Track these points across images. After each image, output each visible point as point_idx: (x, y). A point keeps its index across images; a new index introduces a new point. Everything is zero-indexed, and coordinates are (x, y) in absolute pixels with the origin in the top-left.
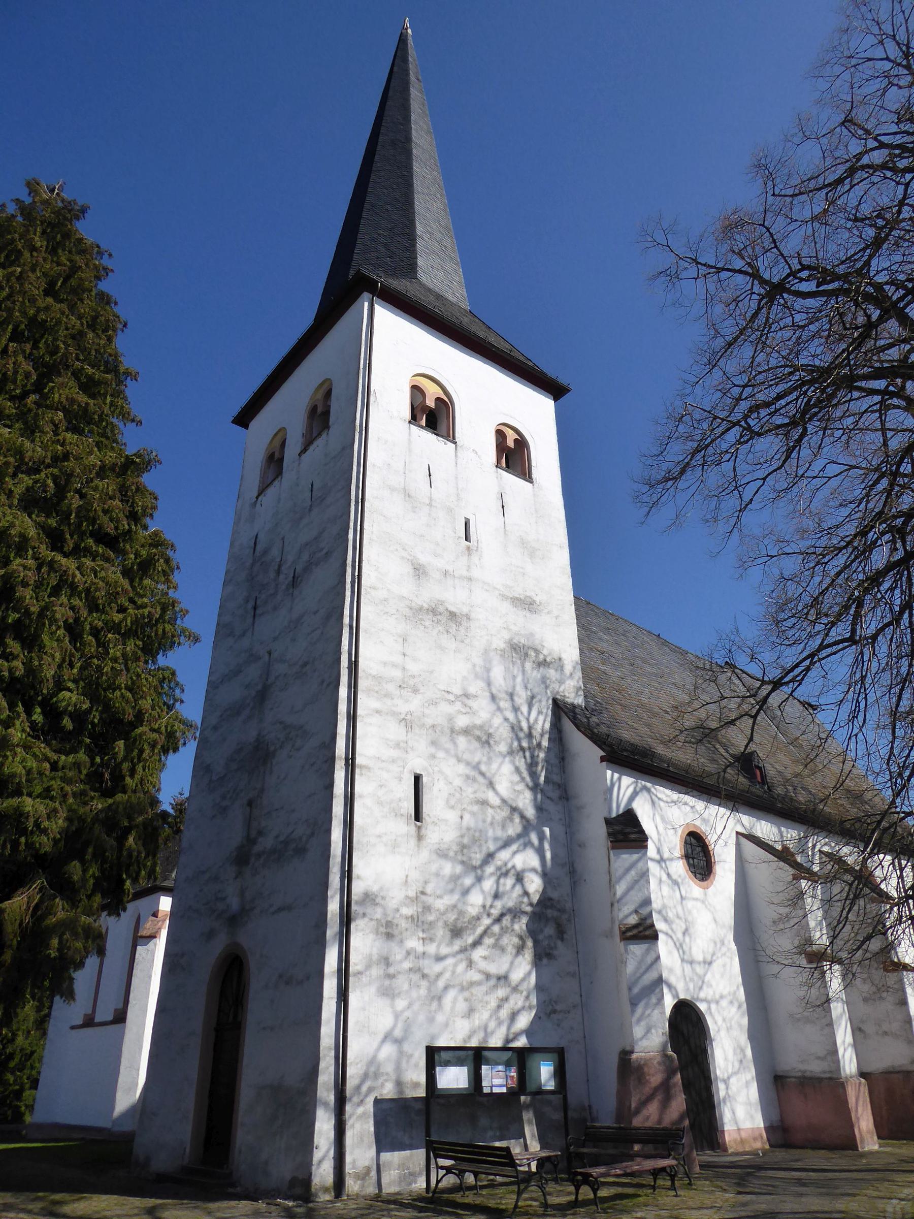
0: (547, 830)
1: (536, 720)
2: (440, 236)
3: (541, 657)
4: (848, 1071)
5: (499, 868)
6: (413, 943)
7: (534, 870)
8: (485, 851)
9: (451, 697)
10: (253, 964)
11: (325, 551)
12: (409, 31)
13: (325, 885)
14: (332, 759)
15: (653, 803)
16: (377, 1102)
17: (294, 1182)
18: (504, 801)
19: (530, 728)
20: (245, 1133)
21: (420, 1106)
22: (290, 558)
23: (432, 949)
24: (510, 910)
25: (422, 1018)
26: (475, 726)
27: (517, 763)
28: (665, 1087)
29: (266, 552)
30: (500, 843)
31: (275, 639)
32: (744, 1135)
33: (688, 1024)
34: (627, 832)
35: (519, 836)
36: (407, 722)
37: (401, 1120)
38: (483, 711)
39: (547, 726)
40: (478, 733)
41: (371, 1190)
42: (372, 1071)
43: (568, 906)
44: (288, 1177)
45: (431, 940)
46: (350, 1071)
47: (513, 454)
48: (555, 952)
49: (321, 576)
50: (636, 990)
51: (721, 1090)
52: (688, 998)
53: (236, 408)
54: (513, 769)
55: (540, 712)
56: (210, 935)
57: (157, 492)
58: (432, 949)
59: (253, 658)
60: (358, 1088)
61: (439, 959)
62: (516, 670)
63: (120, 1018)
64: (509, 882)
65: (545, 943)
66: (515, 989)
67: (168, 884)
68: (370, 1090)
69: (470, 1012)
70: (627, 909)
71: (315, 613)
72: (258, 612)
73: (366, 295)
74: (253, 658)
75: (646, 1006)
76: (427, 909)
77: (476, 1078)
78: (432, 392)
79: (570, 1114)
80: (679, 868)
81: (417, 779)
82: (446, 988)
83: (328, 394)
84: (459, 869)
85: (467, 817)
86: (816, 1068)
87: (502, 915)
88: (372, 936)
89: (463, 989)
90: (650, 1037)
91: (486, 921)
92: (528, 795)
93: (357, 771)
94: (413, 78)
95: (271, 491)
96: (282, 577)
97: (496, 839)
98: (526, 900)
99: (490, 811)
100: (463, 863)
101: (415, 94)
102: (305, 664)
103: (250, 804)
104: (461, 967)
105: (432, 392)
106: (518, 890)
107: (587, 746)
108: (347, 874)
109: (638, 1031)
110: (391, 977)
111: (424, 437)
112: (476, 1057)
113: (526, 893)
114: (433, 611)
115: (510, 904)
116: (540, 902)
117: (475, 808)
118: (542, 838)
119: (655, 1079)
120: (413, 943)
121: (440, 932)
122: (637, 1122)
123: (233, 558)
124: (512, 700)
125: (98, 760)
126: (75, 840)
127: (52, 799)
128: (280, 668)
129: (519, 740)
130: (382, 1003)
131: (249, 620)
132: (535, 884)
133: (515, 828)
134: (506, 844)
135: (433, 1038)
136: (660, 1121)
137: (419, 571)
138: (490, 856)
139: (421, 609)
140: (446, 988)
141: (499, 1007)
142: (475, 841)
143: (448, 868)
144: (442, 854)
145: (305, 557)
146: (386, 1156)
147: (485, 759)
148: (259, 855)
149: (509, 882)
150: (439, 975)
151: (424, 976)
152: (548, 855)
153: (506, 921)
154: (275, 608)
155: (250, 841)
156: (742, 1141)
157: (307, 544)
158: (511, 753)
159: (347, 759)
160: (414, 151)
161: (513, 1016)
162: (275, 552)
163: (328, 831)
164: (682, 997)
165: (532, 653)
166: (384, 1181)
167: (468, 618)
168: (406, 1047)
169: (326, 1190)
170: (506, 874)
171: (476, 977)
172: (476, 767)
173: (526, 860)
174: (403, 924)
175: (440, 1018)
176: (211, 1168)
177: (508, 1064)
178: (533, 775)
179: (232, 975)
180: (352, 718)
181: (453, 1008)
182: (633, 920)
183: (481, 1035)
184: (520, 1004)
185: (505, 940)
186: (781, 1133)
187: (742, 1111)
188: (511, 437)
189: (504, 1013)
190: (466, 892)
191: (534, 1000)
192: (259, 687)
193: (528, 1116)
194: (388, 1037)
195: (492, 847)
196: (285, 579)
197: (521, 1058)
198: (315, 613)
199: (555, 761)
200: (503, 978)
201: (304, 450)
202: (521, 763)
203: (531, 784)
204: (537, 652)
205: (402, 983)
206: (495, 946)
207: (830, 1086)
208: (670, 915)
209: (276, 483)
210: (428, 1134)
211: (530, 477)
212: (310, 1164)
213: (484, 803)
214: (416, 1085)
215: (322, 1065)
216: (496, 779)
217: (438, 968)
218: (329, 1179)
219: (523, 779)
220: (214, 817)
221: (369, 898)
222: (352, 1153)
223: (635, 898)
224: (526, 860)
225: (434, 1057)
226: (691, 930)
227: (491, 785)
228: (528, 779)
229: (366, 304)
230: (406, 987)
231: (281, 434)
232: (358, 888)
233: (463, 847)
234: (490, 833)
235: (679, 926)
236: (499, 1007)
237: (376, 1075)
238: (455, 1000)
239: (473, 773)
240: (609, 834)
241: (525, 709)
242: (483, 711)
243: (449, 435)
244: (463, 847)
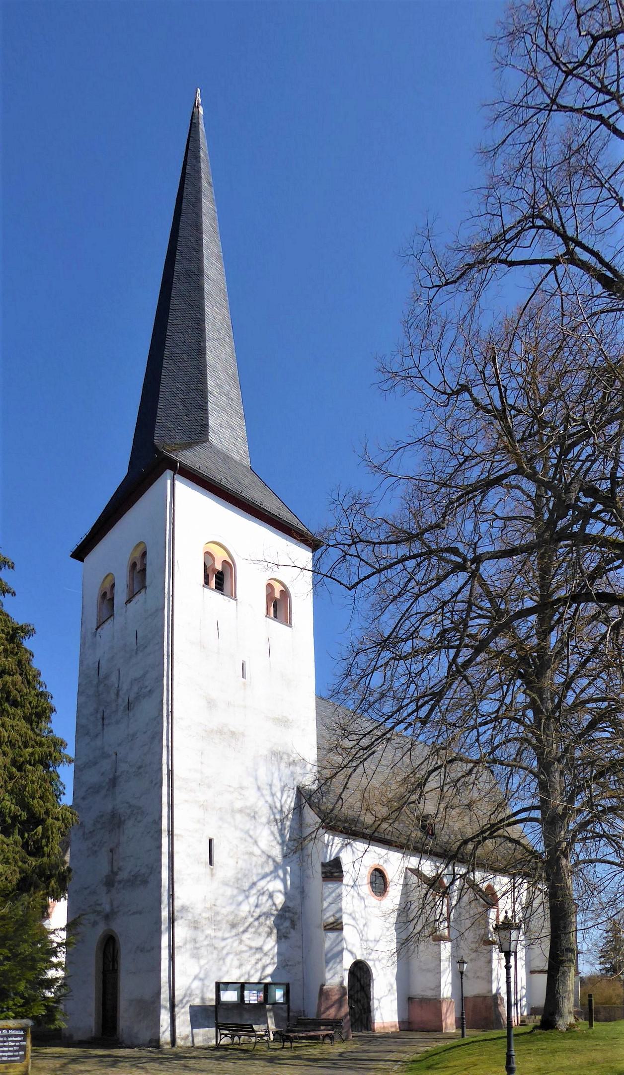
0: (288, 868)
1: (286, 801)
2: (228, 387)
3: (291, 759)
4: (445, 996)
5: (259, 891)
6: (209, 932)
7: (280, 892)
8: (251, 881)
9: (232, 789)
10: (121, 941)
11: (148, 689)
12: (201, 110)
13: (160, 903)
14: (159, 832)
15: (353, 852)
16: (191, 1006)
17: (151, 1041)
18: (263, 852)
19: (282, 806)
20: (125, 1019)
21: (214, 1009)
22: (125, 687)
23: (220, 934)
24: (264, 914)
25: (214, 968)
26: (246, 807)
27: (272, 829)
28: (340, 1002)
29: (107, 677)
30: (260, 877)
31: (119, 745)
32: (386, 1025)
33: (360, 973)
34: (333, 871)
35: (272, 872)
36: (204, 807)
37: (210, 1014)
38: (252, 798)
39: (293, 805)
40: (248, 811)
41: (189, 1044)
42: (189, 993)
43: (299, 911)
44: (148, 1039)
45: (219, 930)
47: (278, 605)
48: (289, 936)
49: (145, 708)
50: (329, 955)
51: (375, 1004)
52: (362, 959)
53: (73, 546)
54: (269, 832)
55: (289, 796)
57: (33, 651)
58: (220, 934)
59: (105, 756)
60: (181, 1001)
61: (224, 939)
62: (274, 769)
64: (265, 898)
65: (284, 931)
66: (266, 954)
68: (188, 1001)
69: (241, 965)
70: (328, 915)
71: (145, 733)
72: (106, 722)
73: (169, 473)
74: (105, 756)
75: (335, 963)
76: (217, 913)
77: (242, 997)
78: (220, 556)
79: (291, 1014)
80: (366, 889)
81: (211, 841)
82: (227, 954)
83: (144, 554)
84: (235, 892)
85: (240, 862)
86: (429, 994)
87: (260, 916)
88: (186, 928)
89: (237, 954)
90: (337, 977)
91: (251, 920)
92: (278, 847)
93: (175, 838)
94: (204, 184)
95: (106, 626)
96: (120, 700)
97: (258, 874)
98: (274, 908)
99: (254, 859)
100: (237, 888)
101: (208, 205)
102: (140, 768)
103: (111, 851)
104: (236, 944)
105: (220, 556)
106: (270, 902)
107: (319, 816)
108: (172, 896)
109: (328, 975)
110: (197, 948)
113: (274, 904)
114: (220, 732)
115: (265, 910)
116: (282, 909)
117: (246, 857)
118: (285, 873)
119: (335, 997)
120: (209, 932)
121: (225, 926)
122: (324, 1017)
123: (82, 674)
124: (271, 788)
125: (26, 835)
127: (10, 863)
128: (123, 767)
129: (274, 814)
130: (193, 961)
131: (100, 727)
132: (280, 899)
133: (270, 867)
134: (264, 877)
135: (221, 978)
136: (336, 1016)
137: (211, 704)
138: (254, 884)
139: (212, 731)
140: (227, 954)
141: (256, 963)
142: (245, 876)
143: (229, 892)
144: (226, 884)
145: (135, 689)
146: (195, 1030)
147: (252, 827)
148: (120, 882)
149: (265, 898)
150: (223, 948)
151: (215, 948)
152: (289, 883)
153: (262, 919)
154: (117, 722)
155: (114, 873)
156: (384, 1028)
157: (136, 680)
158: (269, 822)
159: (169, 831)
160: (206, 286)
161: (264, 968)
162: (114, 678)
163: (160, 873)
164: (359, 958)
165: (285, 757)
166: (196, 1041)
167: (243, 735)
168: (206, 982)
169: (167, 1044)
170: (263, 894)
171: (245, 948)
172: (247, 832)
173: (278, 885)
174: (204, 922)
175: (224, 969)
176: (107, 1034)
177: (258, 991)
178: (282, 835)
179: (109, 947)
180: (171, 806)
181: (231, 965)
182: (331, 920)
183: (246, 976)
184: (268, 962)
185: (261, 930)
186: (407, 1025)
187: (386, 1012)
188: (278, 588)
189: (259, 966)
190: (240, 904)
191: (276, 960)
192: (111, 776)
193: (270, 1014)
194: (196, 977)
195: (255, 880)
196: (122, 702)
197: (266, 988)
198: (145, 733)
199: (296, 827)
200: (259, 949)
201: (129, 601)
202: (275, 829)
203: (280, 841)
204: (289, 756)
205: (203, 951)
206: (255, 932)
207: (434, 1003)
208: (357, 916)
209: (109, 621)
210: (216, 1019)
211: (290, 623)
212: (159, 1033)
213: (251, 854)
214: (212, 1000)
215: (163, 990)
216: (259, 840)
217: (223, 944)
218: (169, 1039)
219: (276, 838)
220: (88, 856)
221: (184, 908)
222: (180, 1028)
223: (334, 908)
224: (278, 885)
226: (369, 924)
227: (256, 842)
228: (279, 838)
229: (169, 482)
230: (205, 953)
231: (109, 578)
232: (178, 904)
233: (238, 880)
234: (254, 871)
235: (361, 922)
236: (256, 963)
237: (191, 995)
238: (232, 960)
239: (246, 836)
240: (323, 873)
241: (279, 794)
242: (252, 798)
243: (233, 596)
244: (238, 880)
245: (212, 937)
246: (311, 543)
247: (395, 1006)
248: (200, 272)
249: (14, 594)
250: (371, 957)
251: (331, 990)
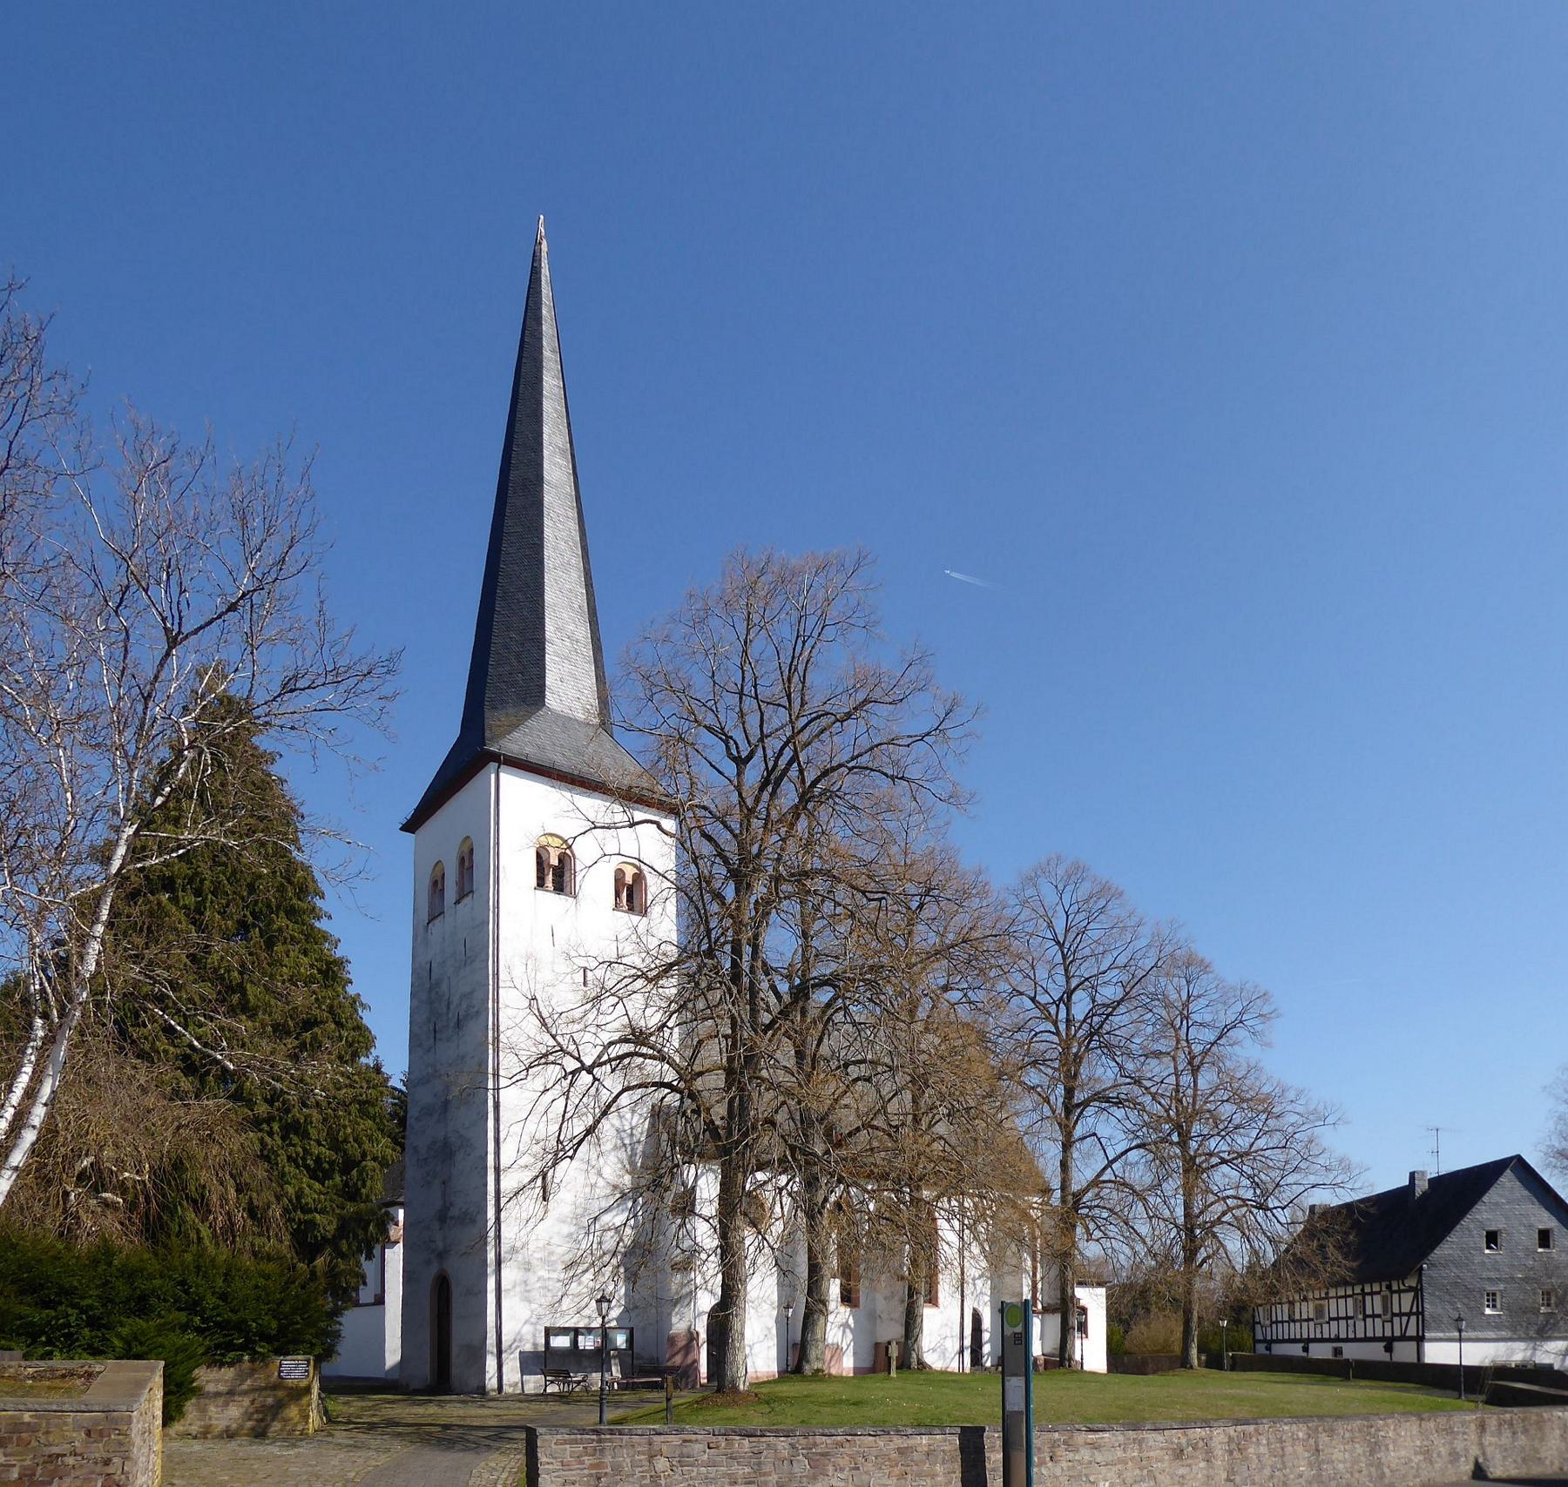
10: (453, 1283)
29: (438, 984)
37: (530, 1362)
42: (518, 1338)
46: (504, 1338)
47: (630, 893)
56: (428, 1263)
63: (380, 1300)
67: (401, 1199)
76: (551, 1253)
77: (575, 1342)
84: (573, 1229)
94: (547, 353)
95: (436, 922)
108: (498, 1237)
109: (674, 1320)
111: (549, 899)
112: (576, 1332)
126: (344, 1228)
158: (615, 1148)
162: (444, 987)
174: (534, 1262)
179: (443, 1288)
222: (507, 1375)
225: (549, 1332)
246: (673, 811)
247: (774, 1352)
248: (539, 479)
249: (330, 917)
251: (677, 1335)
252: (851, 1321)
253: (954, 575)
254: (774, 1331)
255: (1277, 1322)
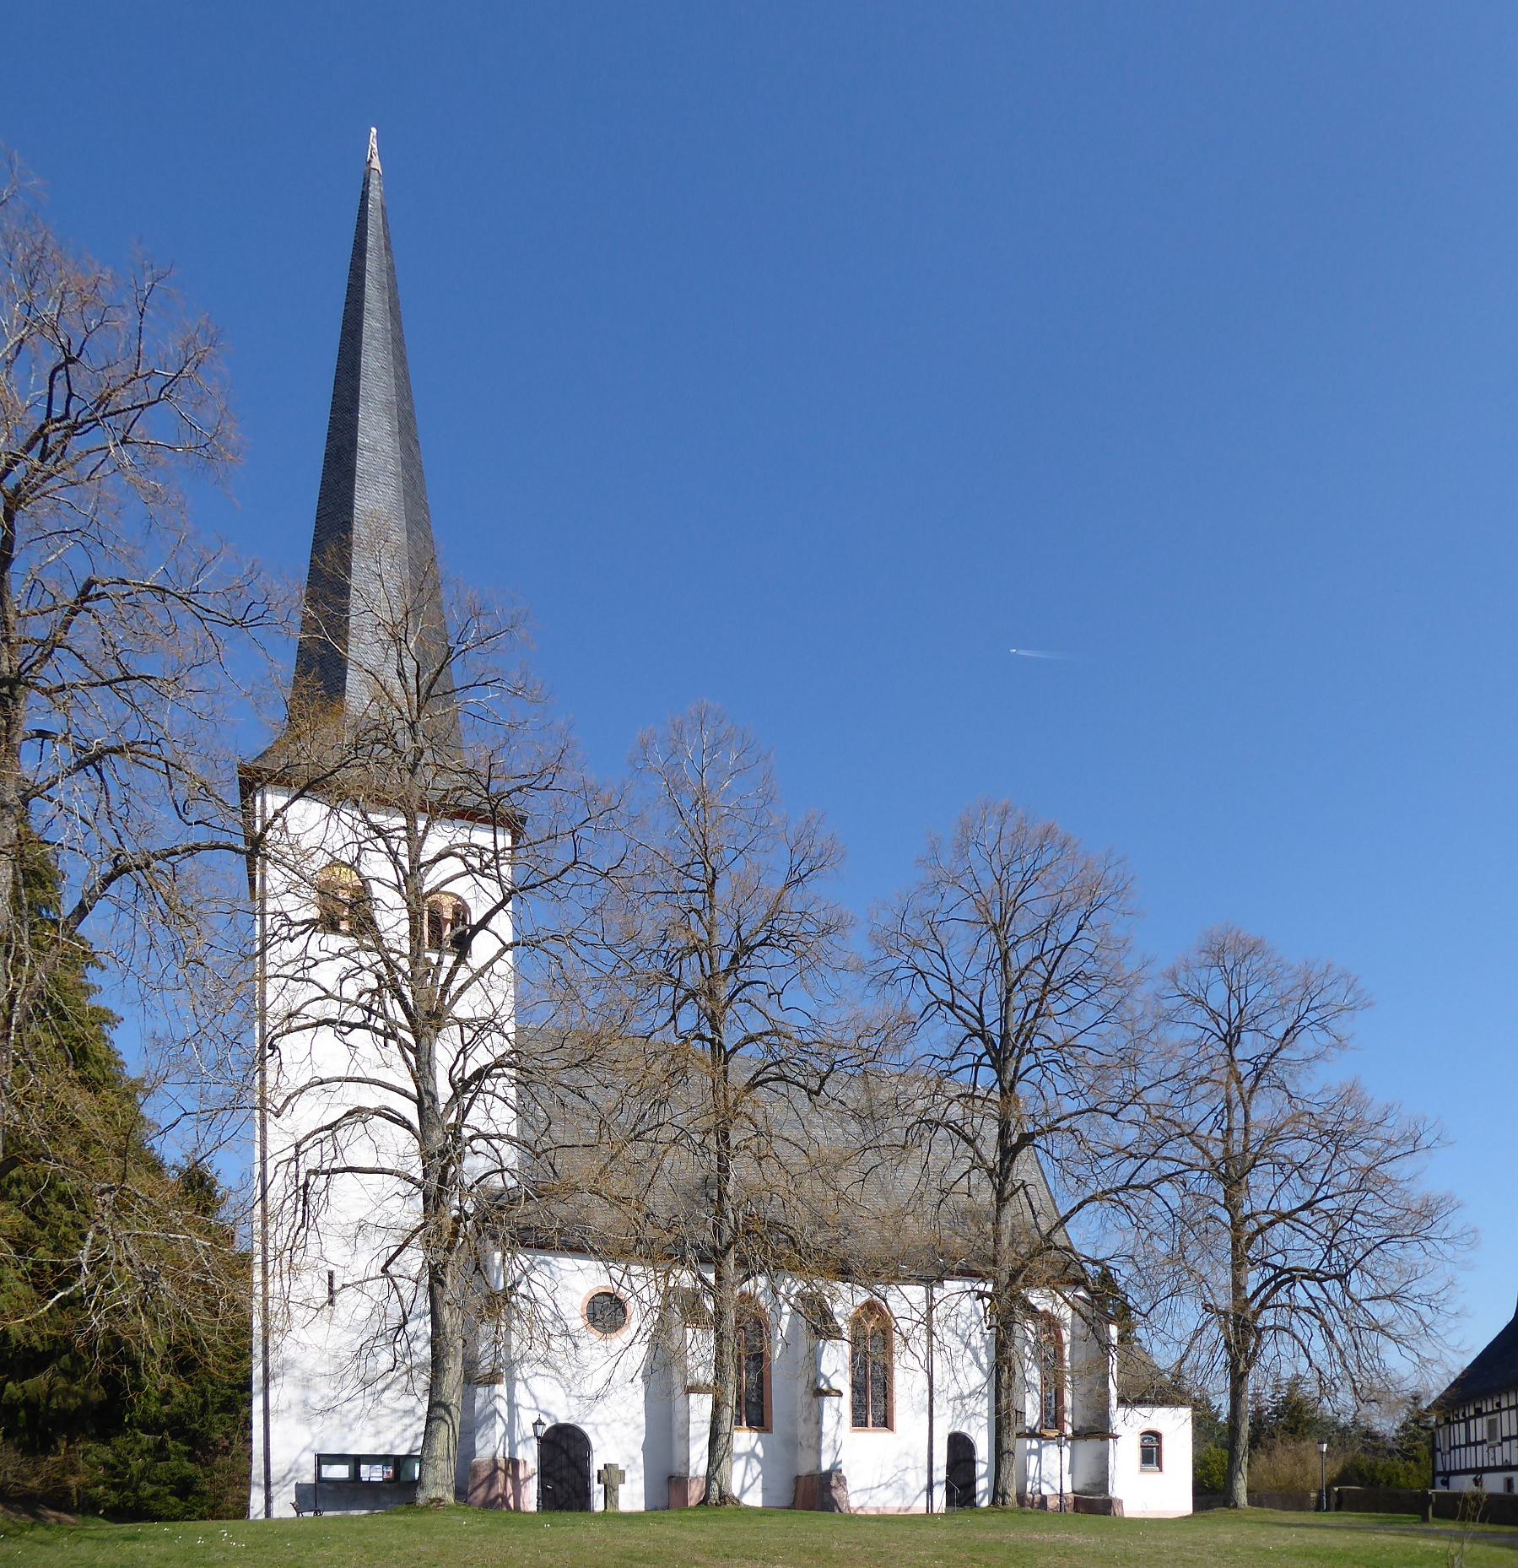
42: (295, 1468)
46: (273, 1469)
109: (478, 1445)
112: (356, 1461)
225: (323, 1459)
237: (297, 1471)
245: (324, 1394)
250: (588, 1420)
251: (480, 1463)
252: (759, 1450)
253: (1022, 652)
254: (641, 1461)
255: (1455, 1447)
